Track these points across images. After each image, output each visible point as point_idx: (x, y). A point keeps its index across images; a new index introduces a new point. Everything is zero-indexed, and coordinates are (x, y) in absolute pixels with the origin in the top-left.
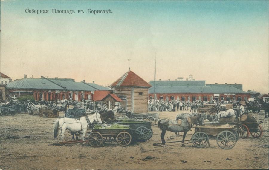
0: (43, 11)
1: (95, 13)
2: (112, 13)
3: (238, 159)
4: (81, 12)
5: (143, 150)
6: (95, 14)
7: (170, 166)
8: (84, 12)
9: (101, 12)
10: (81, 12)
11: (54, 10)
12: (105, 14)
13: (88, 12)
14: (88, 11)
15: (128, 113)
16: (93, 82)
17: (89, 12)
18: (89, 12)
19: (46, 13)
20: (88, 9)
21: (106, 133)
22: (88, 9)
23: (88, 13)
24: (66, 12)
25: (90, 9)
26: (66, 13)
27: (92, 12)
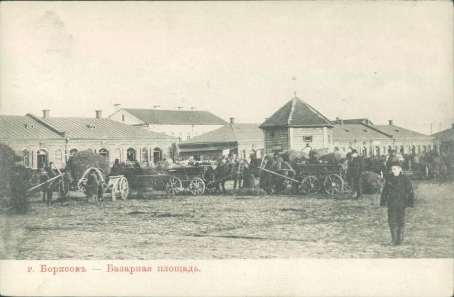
0: (163, 269)
1: (55, 271)
2: (200, 271)
3: (180, 240)
4: (81, 270)
5: (36, 240)
6: (131, 273)
7: (102, 237)
8: (86, 270)
9: (67, 270)
10: (81, 270)
11: (160, 269)
12: (169, 266)
13: (107, 270)
14: (42, 268)
15: (369, 190)
16: (390, 122)
17: (111, 270)
18: (111, 270)
19: (147, 272)
20: (42, 266)
21: (331, 172)
22: (109, 265)
23: (109, 271)
24: (182, 270)
25: (112, 265)
26: (181, 271)
27: (50, 270)
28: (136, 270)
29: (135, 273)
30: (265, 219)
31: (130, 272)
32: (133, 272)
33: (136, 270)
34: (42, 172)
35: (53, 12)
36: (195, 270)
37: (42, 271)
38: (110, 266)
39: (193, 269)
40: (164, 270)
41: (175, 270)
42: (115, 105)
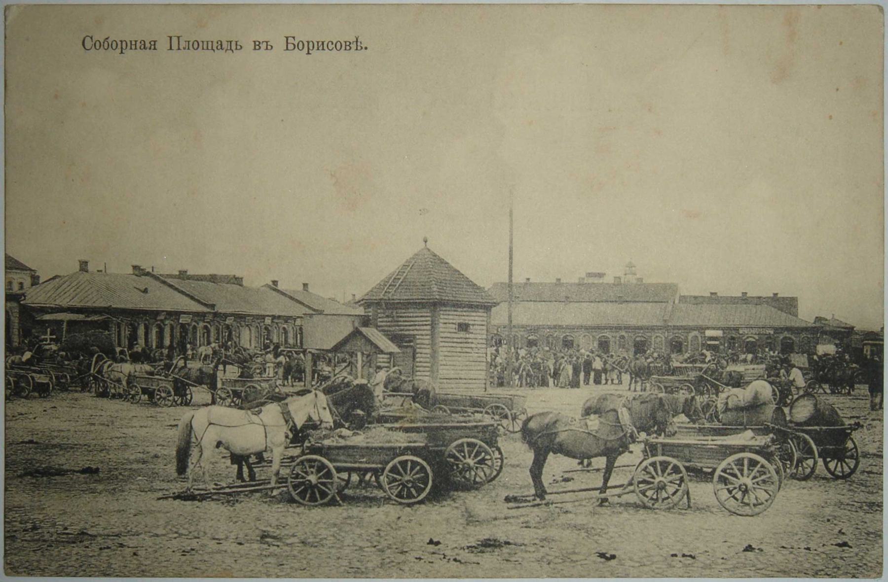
4: (264, 46)
6: (308, 53)
9: (330, 46)
10: (264, 46)
17: (291, 47)
22: (287, 38)
24: (215, 48)
25: (294, 38)
28: (191, 43)
29: (314, 52)
30: (275, 363)
31: (119, 50)
32: (124, 51)
33: (191, 43)
34: (760, 415)
35: (555, 422)
36: (236, 49)
37: (155, 42)
38: (291, 40)
39: (233, 47)
40: (184, 48)
41: (212, 42)
42: (602, 555)
